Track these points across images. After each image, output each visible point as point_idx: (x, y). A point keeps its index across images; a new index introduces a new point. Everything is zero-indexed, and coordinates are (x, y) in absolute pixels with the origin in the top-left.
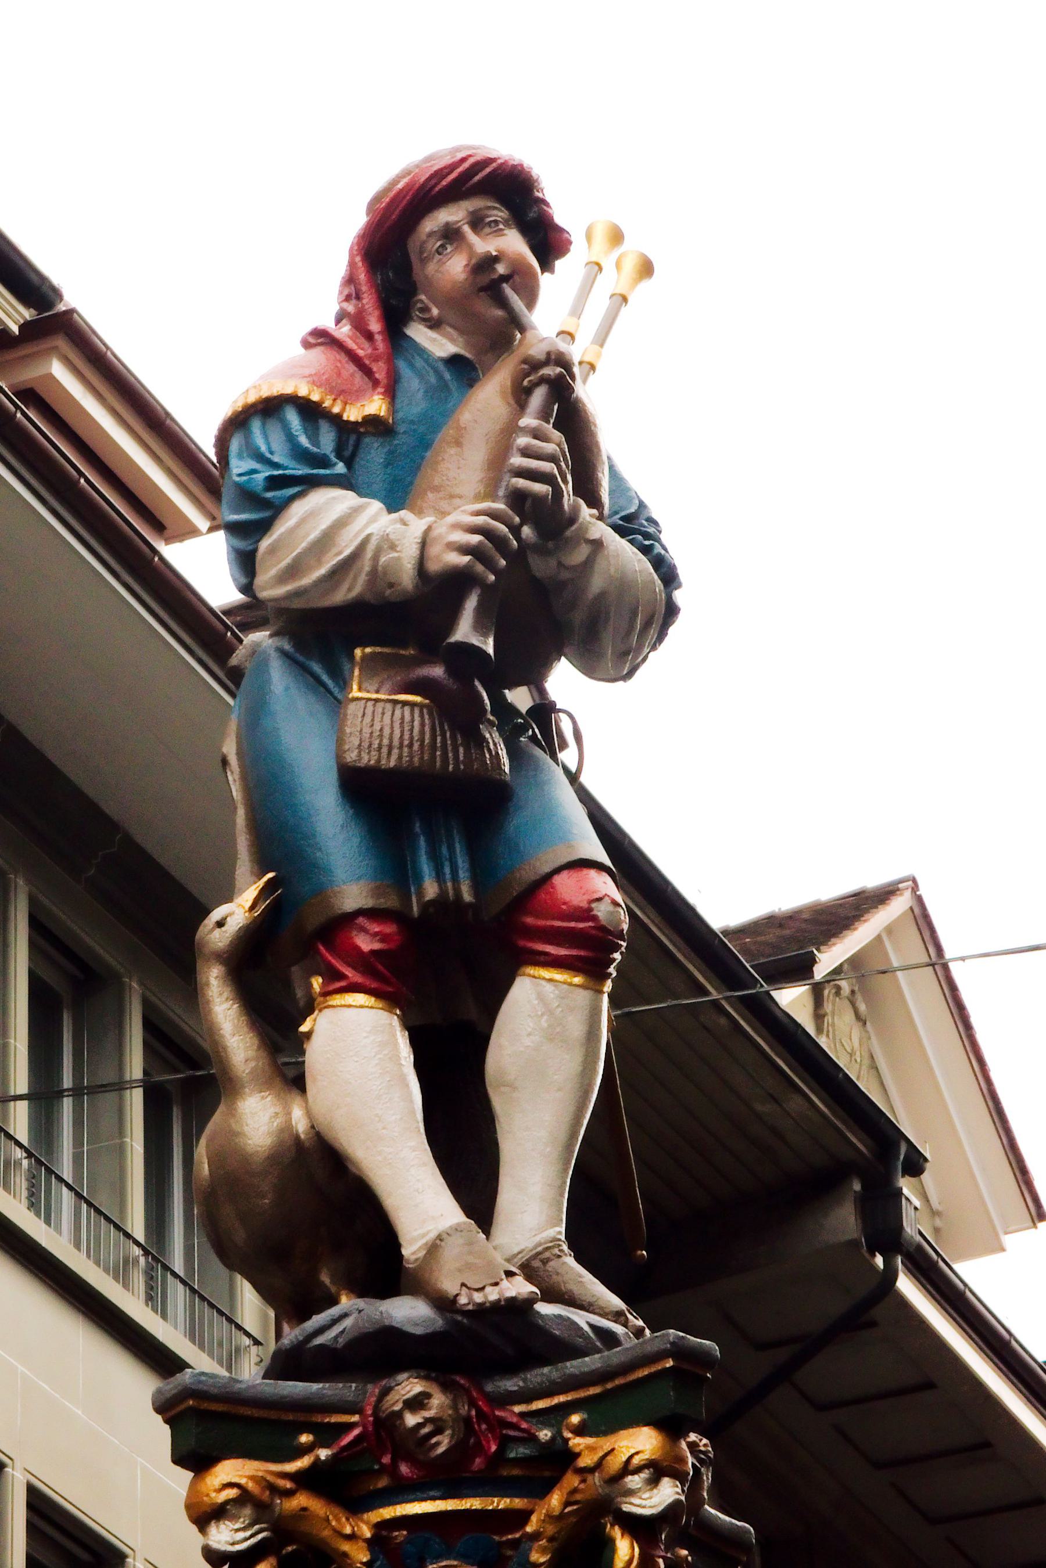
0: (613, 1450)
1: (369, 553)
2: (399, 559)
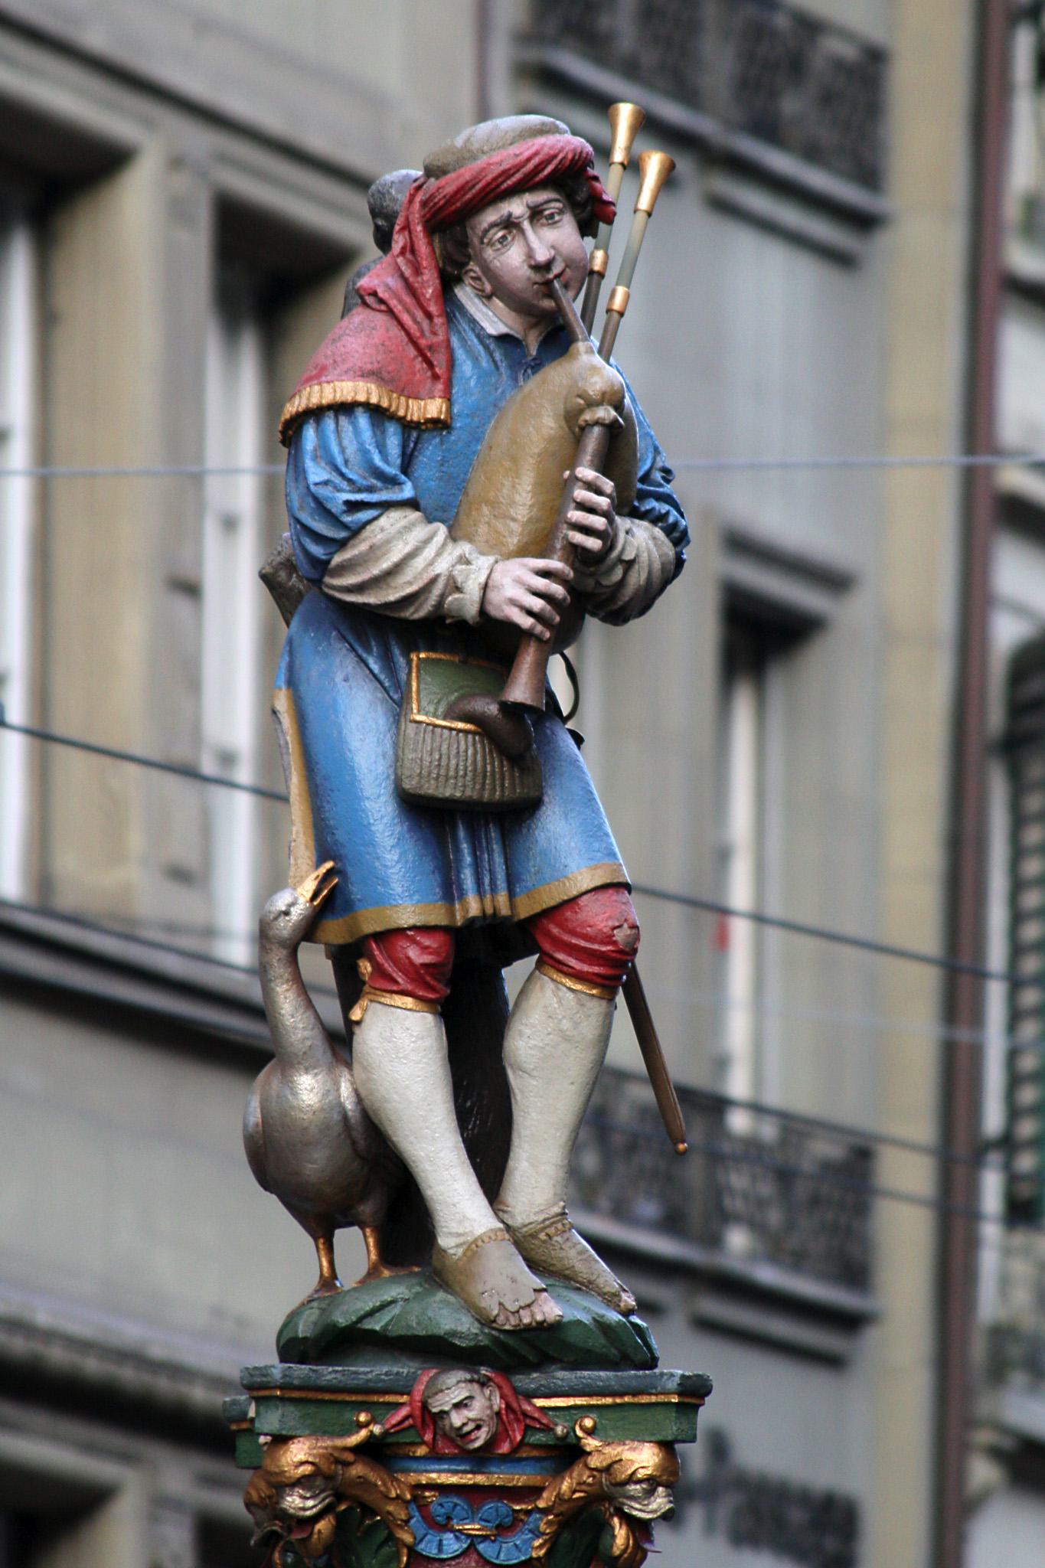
1: (437, 591)
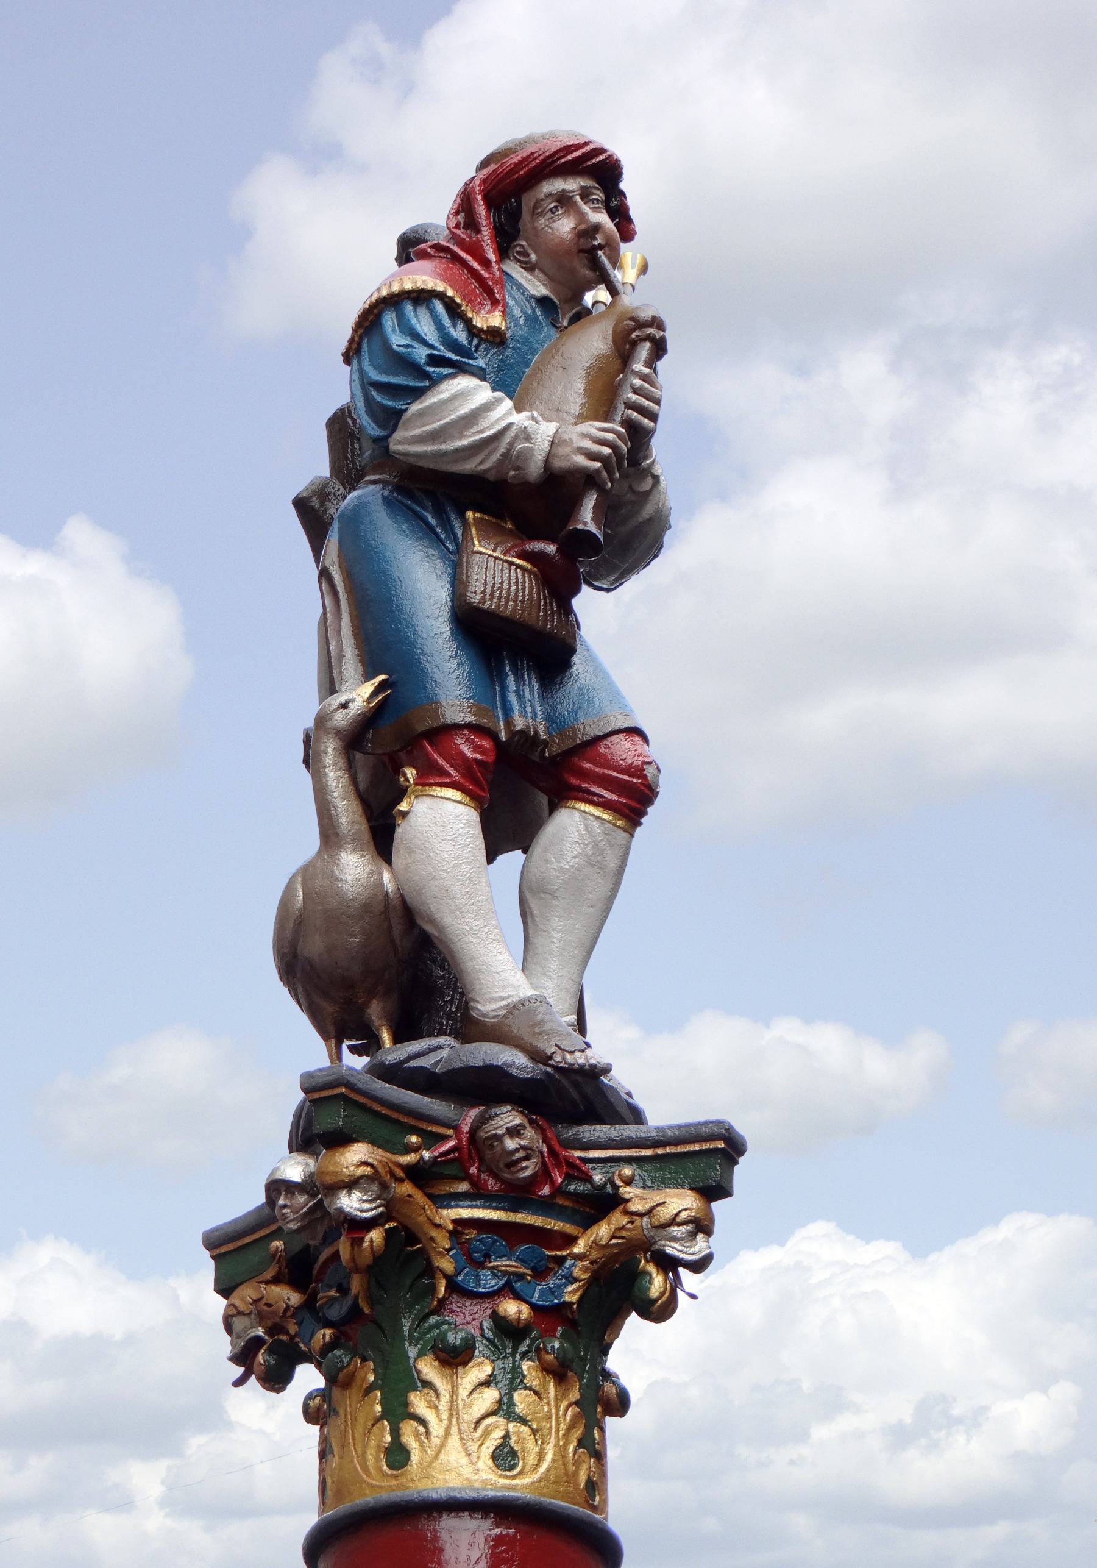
0: (664, 1203)
1: (507, 439)
2: (531, 449)
